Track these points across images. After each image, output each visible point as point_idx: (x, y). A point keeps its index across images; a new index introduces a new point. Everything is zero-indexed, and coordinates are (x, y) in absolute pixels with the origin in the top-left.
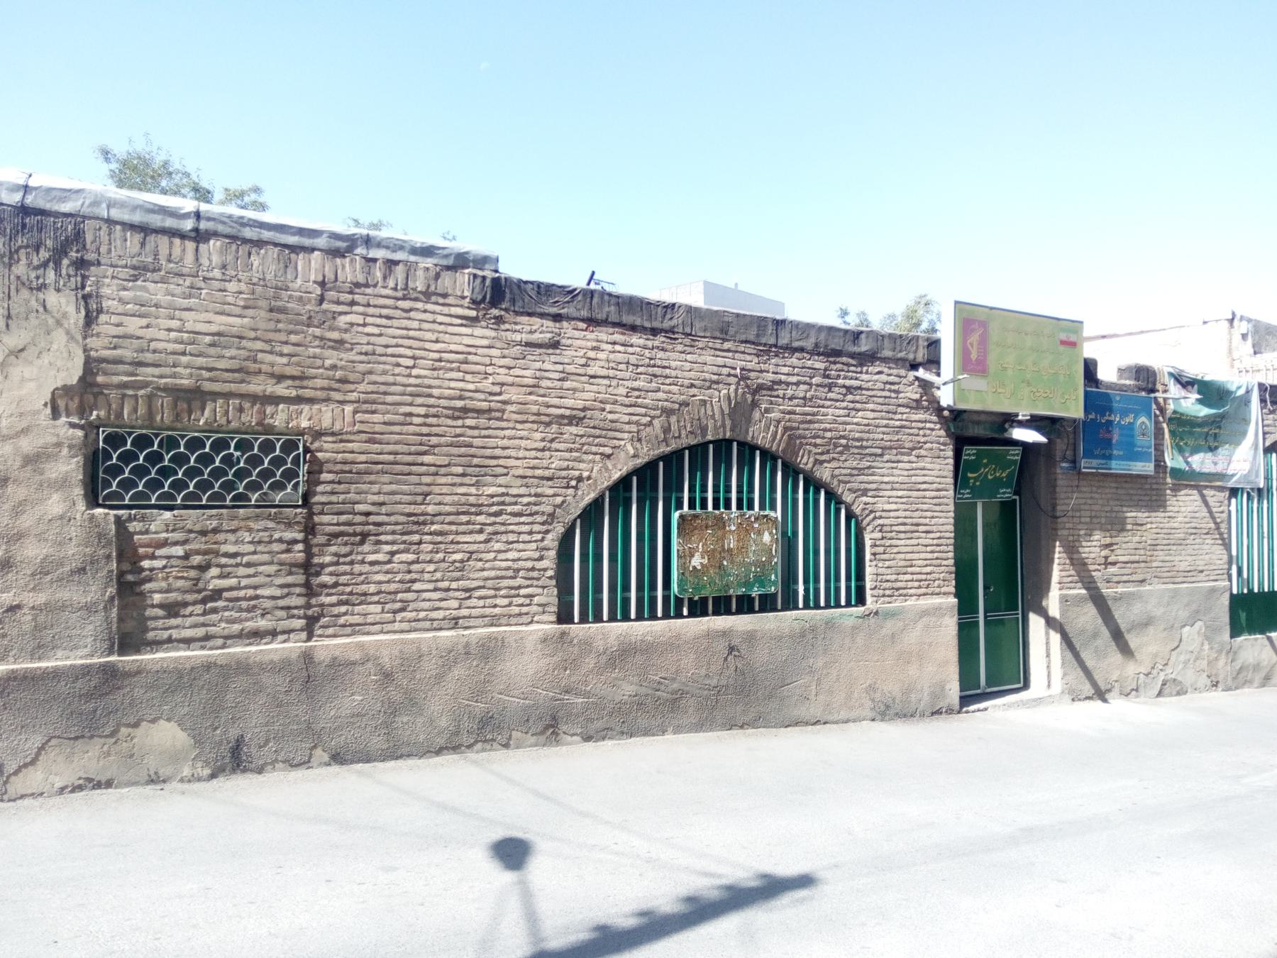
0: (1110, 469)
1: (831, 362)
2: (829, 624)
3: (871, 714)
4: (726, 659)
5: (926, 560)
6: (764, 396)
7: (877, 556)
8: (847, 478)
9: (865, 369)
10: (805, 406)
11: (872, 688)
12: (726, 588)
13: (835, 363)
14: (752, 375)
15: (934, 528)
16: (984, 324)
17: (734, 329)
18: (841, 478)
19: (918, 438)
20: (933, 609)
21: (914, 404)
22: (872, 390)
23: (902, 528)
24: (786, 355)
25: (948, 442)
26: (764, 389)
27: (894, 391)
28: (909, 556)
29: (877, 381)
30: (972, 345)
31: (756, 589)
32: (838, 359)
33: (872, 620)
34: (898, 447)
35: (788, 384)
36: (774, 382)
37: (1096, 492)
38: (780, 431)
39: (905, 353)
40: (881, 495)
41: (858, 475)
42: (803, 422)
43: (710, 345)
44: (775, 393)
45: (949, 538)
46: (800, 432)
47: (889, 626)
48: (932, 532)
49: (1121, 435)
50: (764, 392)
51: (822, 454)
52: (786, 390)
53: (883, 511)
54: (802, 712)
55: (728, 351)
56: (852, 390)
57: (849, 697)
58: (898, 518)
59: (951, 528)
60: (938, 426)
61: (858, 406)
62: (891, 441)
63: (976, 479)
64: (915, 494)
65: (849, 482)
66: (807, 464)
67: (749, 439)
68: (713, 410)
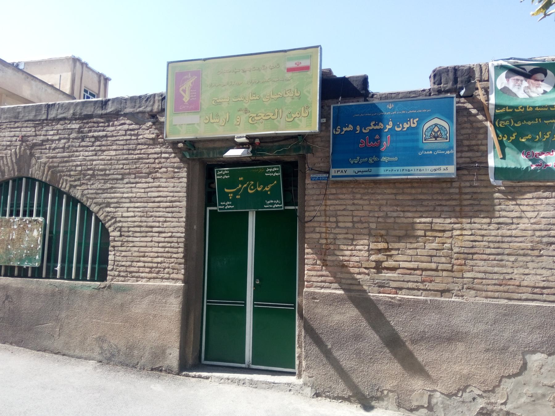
0: (378, 175)
1: (84, 123)
2: (72, 290)
3: (99, 358)
4: (4, 302)
5: (157, 252)
6: (37, 149)
7: (116, 248)
8: (93, 196)
9: (111, 123)
10: (64, 152)
11: (101, 340)
12: (9, 261)
13: (87, 123)
14: (30, 138)
15: (167, 230)
16: (198, 74)
17: (22, 115)
18: (88, 196)
19: (154, 165)
20: (160, 289)
21: (151, 142)
22: (116, 136)
23: (138, 229)
24: (54, 124)
25: (182, 166)
26: (37, 146)
27: (134, 135)
28: (142, 249)
29: (120, 130)
30: (184, 91)
31: (26, 263)
32: (90, 121)
33: (106, 292)
34: (137, 173)
35: (53, 141)
36: (43, 141)
37: (361, 199)
38: (46, 170)
39: (143, 107)
40: (121, 206)
41: (102, 193)
42: (61, 162)
43: (8, 126)
44: (44, 147)
45: (180, 237)
46: (59, 168)
47: (119, 298)
48: (165, 232)
49: (392, 142)
50: (38, 147)
51: (75, 181)
52: (51, 144)
53: (122, 217)
54: (47, 343)
55: (18, 127)
56: (100, 139)
57: (82, 342)
58: (135, 222)
59: (183, 230)
60: (173, 155)
61: (104, 148)
62: (130, 169)
63: (235, 194)
64: (151, 205)
65: (95, 198)
66: (65, 188)
67: (30, 176)
68: (7, 161)
